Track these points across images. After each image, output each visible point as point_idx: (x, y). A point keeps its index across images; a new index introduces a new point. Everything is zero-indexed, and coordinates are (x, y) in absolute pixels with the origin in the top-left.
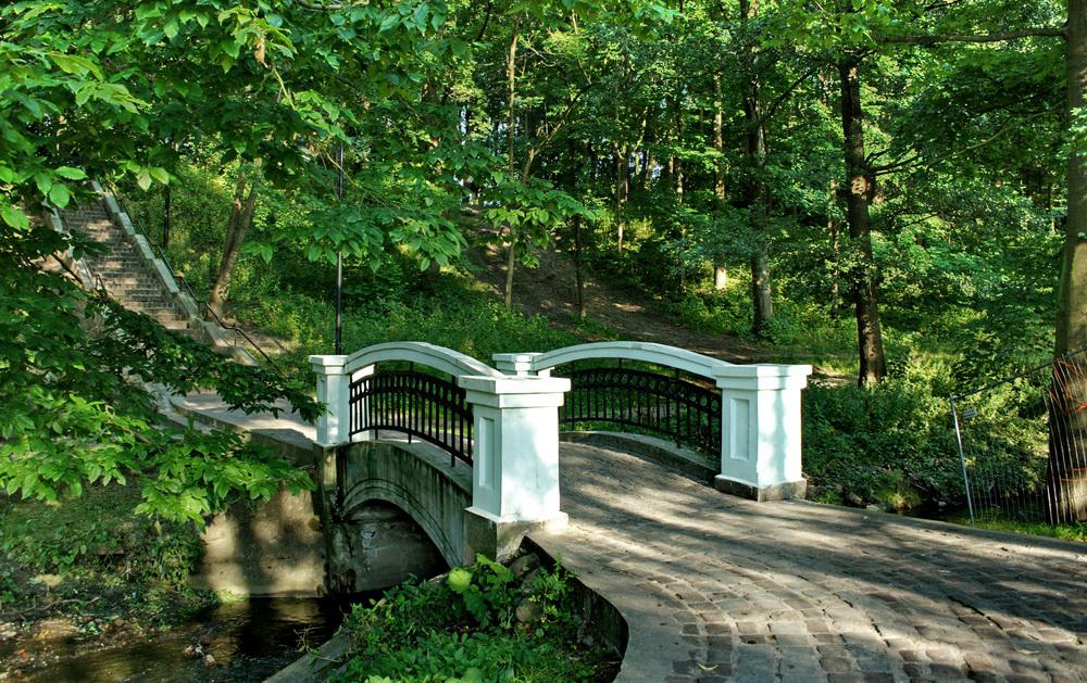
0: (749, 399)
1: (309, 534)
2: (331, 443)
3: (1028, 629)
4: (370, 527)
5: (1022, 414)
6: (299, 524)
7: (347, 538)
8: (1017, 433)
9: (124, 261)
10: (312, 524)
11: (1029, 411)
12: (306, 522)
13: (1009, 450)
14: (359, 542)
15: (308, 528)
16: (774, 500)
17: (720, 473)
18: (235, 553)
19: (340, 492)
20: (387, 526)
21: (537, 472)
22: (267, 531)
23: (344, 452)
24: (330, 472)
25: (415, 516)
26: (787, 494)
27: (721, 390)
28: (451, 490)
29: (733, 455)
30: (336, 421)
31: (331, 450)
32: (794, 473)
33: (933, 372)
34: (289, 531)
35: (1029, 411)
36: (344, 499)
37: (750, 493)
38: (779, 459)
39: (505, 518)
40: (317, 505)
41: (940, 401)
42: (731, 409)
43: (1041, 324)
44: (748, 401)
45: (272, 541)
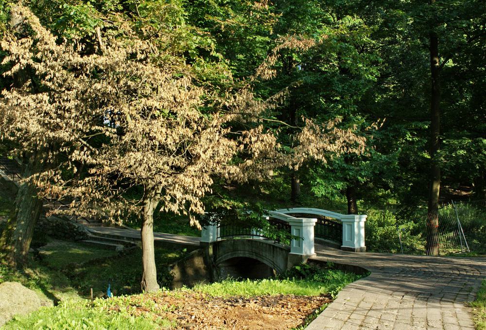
0: (351, 226)
1: (203, 271)
2: (210, 241)
3: (430, 264)
4: (223, 269)
5: (411, 234)
6: (200, 268)
7: (217, 272)
8: (410, 241)
9: (7, 164)
10: (204, 268)
11: (414, 232)
12: (202, 268)
13: (408, 247)
14: (220, 274)
15: (203, 270)
16: (359, 252)
17: (342, 245)
18: (181, 278)
19: (215, 257)
20: (227, 268)
21: (310, 242)
22: (190, 271)
23: (216, 245)
24: (211, 251)
25: (259, 259)
26: (361, 250)
27: (342, 222)
28: (278, 249)
29: (346, 240)
30: (212, 234)
31: (211, 243)
32: (363, 245)
33: (377, 218)
34: (197, 271)
35: (414, 232)
36: (216, 259)
37: (353, 250)
38: (359, 241)
39: (304, 254)
40: (205, 262)
41: (381, 228)
42: (346, 228)
43: (157, 93)
44: (351, 225)
45: (192, 274)
